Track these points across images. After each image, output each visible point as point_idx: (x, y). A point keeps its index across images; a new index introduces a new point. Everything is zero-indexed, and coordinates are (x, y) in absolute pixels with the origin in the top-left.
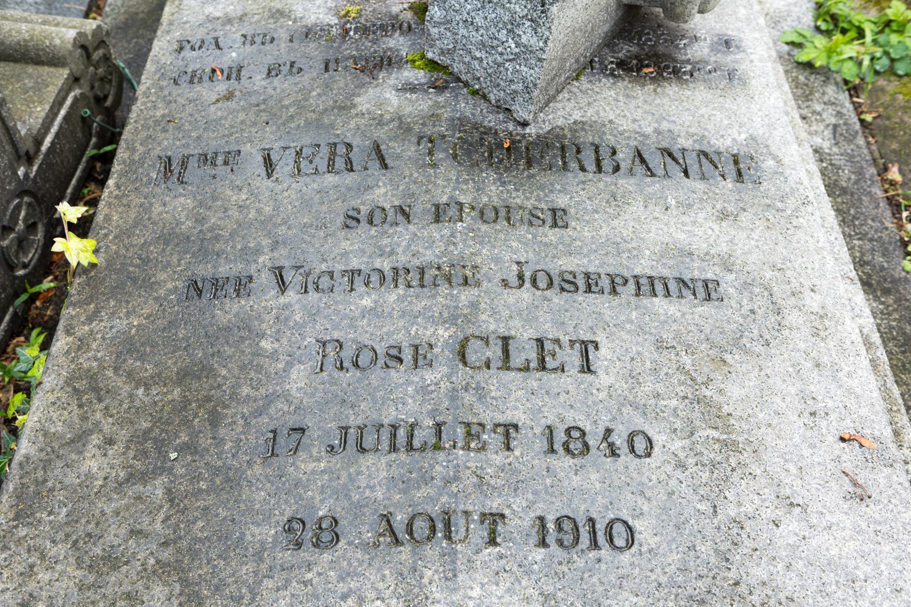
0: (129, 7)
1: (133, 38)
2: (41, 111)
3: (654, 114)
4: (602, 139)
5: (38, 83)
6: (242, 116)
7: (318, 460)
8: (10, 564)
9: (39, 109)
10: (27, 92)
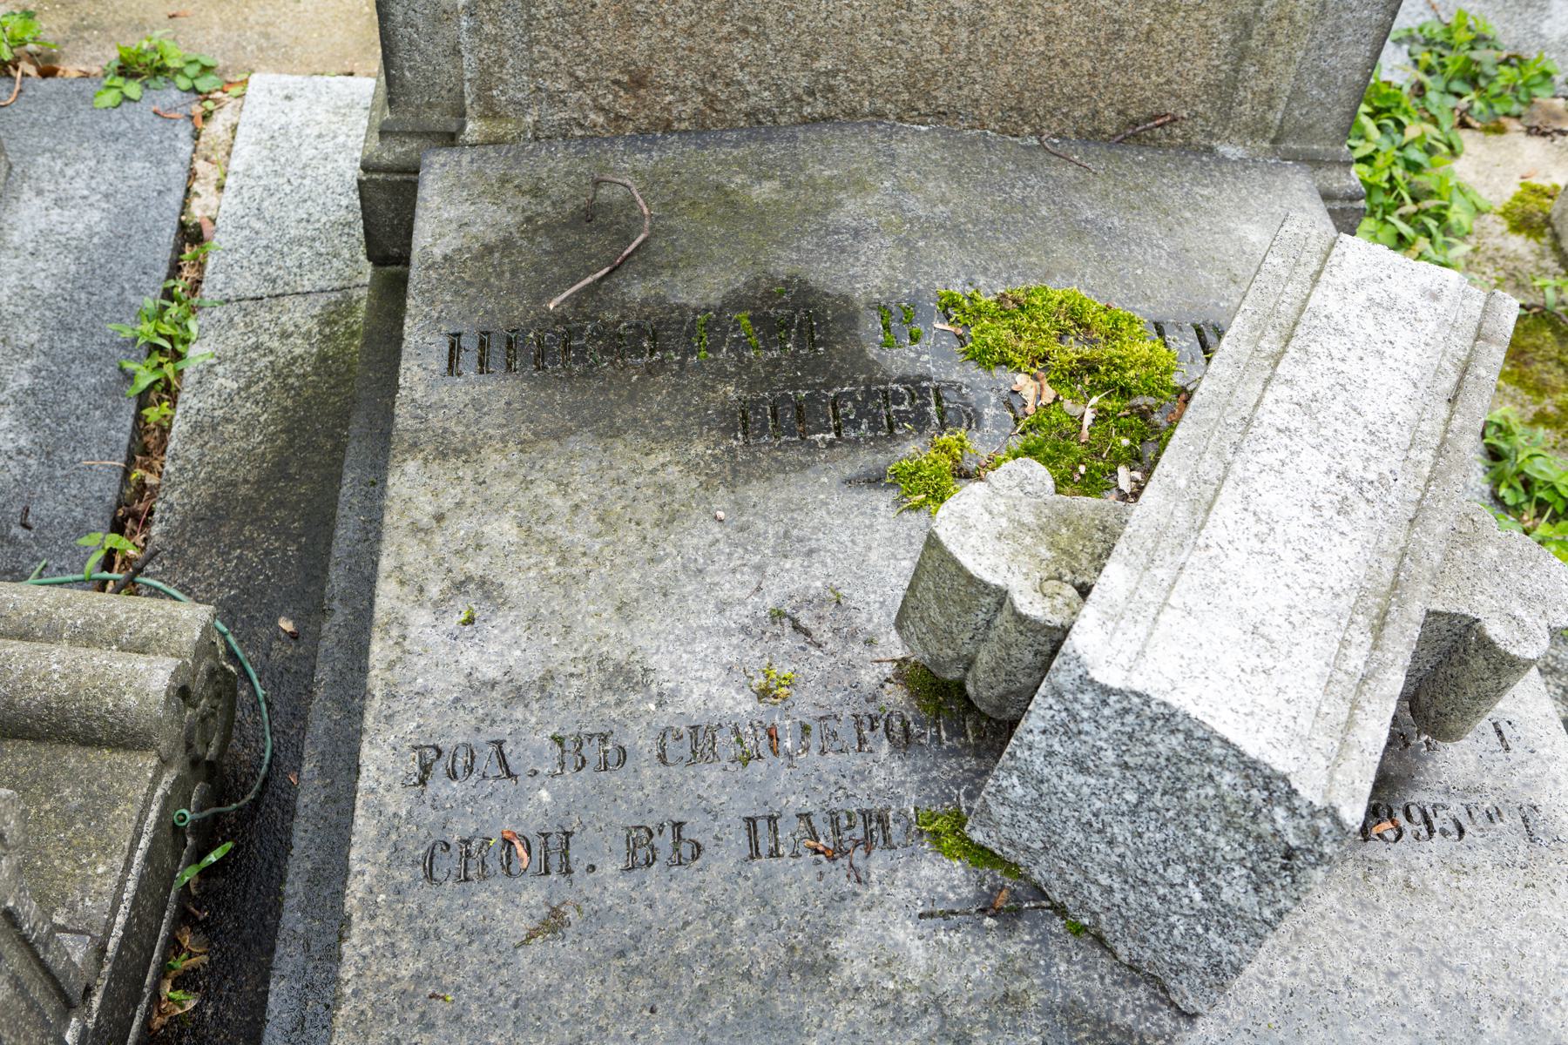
0: (216, 465)
1: (231, 547)
5: (91, 795)
6: (593, 990)
9: (101, 869)
10: (71, 822)
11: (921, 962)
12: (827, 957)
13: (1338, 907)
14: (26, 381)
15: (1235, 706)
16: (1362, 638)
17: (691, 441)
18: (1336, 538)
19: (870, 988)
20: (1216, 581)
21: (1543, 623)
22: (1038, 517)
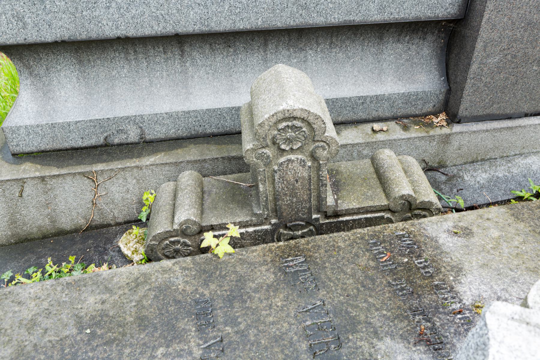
2: (354, 205)
12: (382, 337)
14: (500, 175)
19: (375, 351)
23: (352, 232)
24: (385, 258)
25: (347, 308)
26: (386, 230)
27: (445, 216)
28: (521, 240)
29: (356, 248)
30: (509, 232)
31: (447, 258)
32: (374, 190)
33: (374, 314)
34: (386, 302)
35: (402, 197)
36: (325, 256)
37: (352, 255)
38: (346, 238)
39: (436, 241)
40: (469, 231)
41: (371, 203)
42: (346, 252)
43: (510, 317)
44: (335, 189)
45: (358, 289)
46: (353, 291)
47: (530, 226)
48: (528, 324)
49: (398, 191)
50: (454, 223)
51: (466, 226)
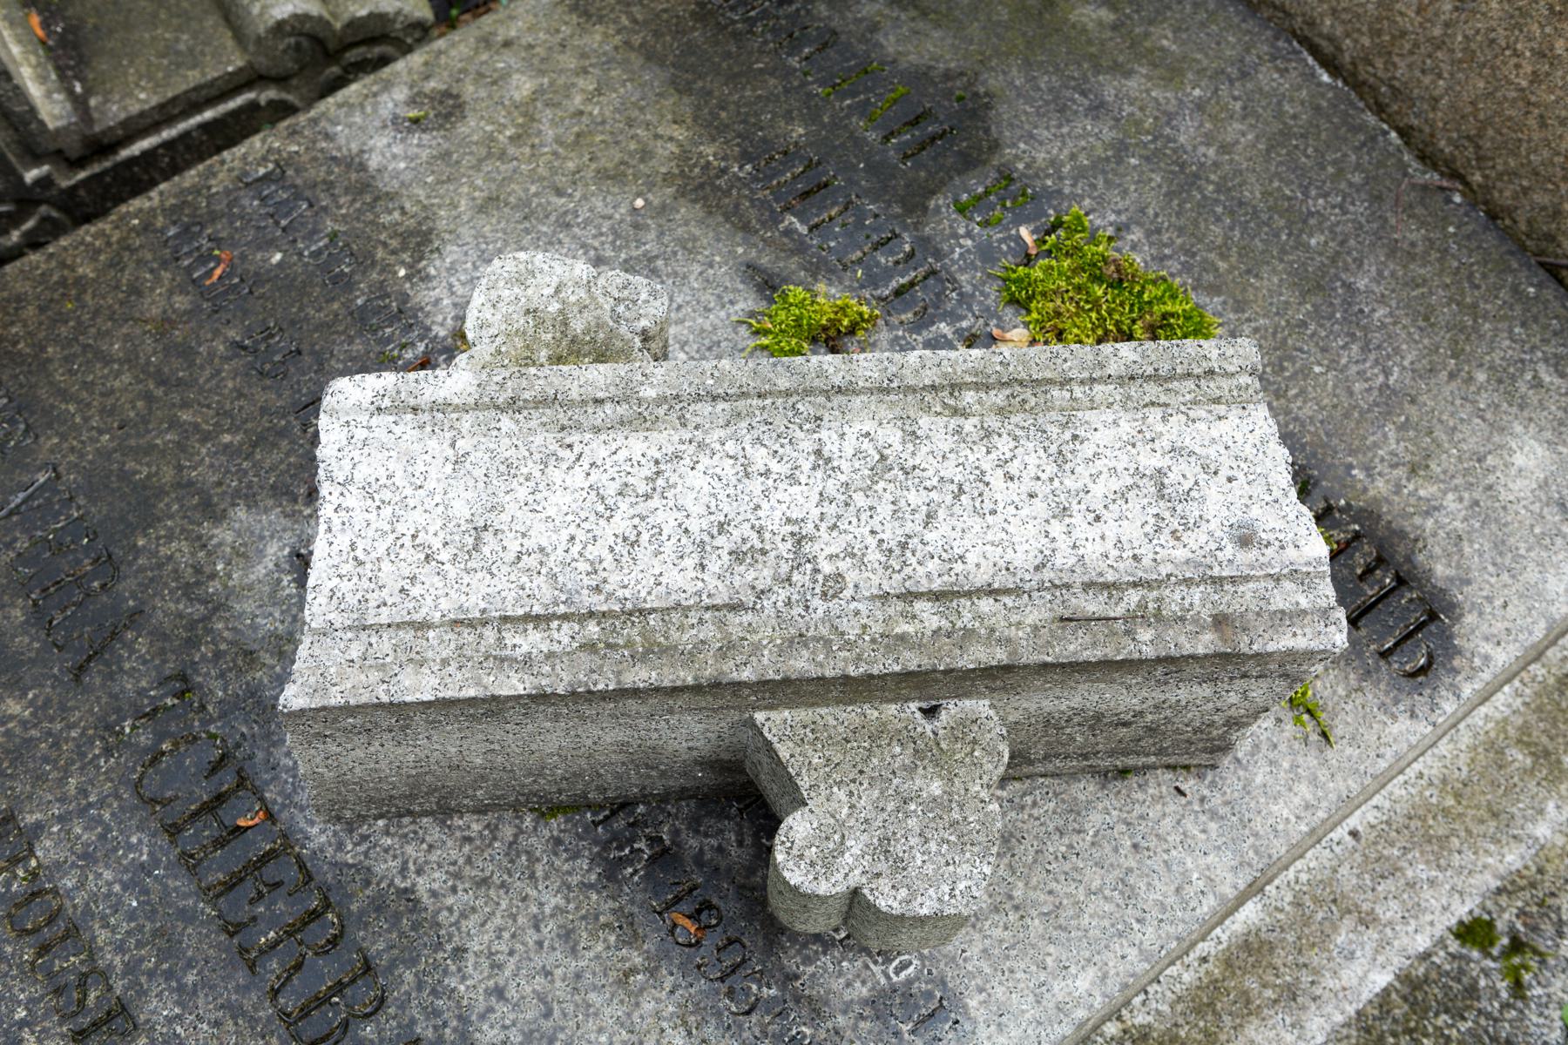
2: (144, 99)
3: (548, 1014)
4: (393, 964)
7: (1385, 435)
8: (1468, 138)
11: (253, 577)
13: (547, 910)
15: (360, 545)
16: (566, 640)
17: (714, 140)
18: (689, 563)
19: (209, 554)
20: (525, 471)
21: (856, 879)
22: (586, 331)
23: (113, 217)
24: (218, 272)
25: (124, 464)
26: (214, 175)
27: (386, 72)
28: (591, 88)
29: (132, 265)
30: (561, 71)
31: (390, 213)
32: (194, 25)
33: (198, 453)
34: (228, 407)
35: (280, 28)
36: (41, 324)
37: (121, 296)
38: (97, 243)
39: (363, 167)
40: (451, 102)
41: (193, 77)
42: (104, 288)
43: (372, 408)
44: (71, 58)
45: (149, 397)
46: (134, 407)
47: (619, 32)
48: (415, 410)
49: (261, 14)
50: (411, 87)
51: (443, 87)
